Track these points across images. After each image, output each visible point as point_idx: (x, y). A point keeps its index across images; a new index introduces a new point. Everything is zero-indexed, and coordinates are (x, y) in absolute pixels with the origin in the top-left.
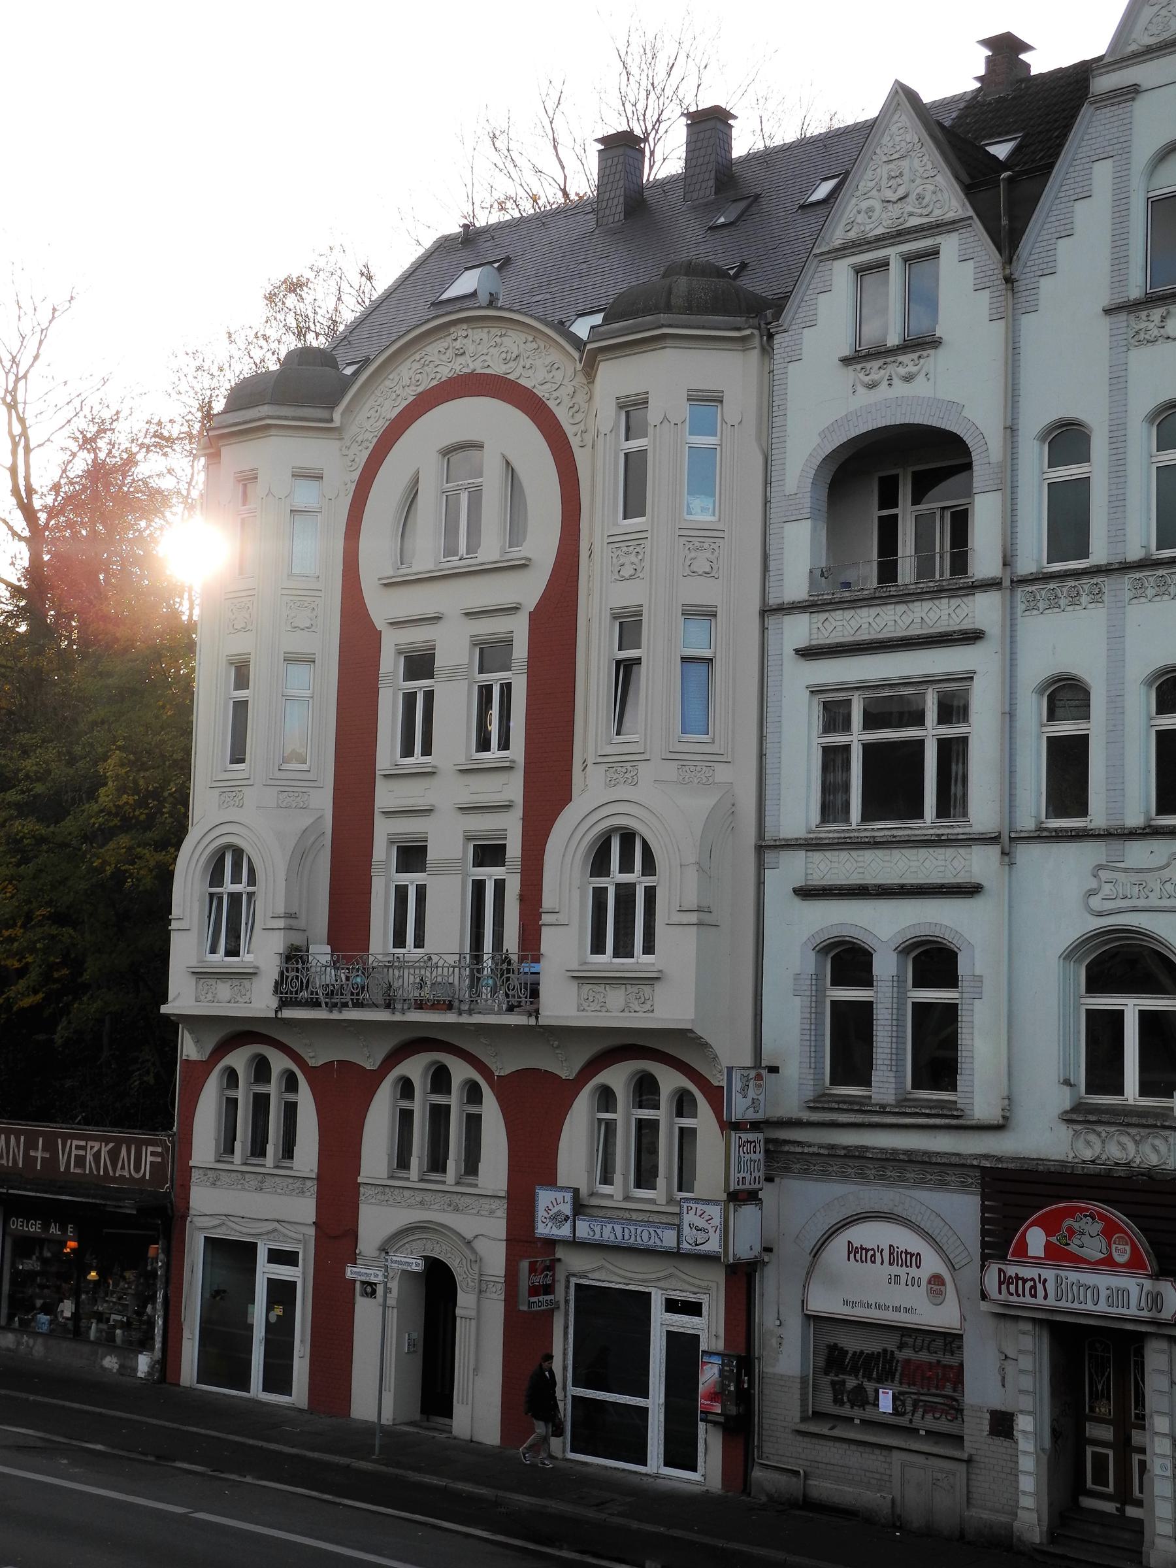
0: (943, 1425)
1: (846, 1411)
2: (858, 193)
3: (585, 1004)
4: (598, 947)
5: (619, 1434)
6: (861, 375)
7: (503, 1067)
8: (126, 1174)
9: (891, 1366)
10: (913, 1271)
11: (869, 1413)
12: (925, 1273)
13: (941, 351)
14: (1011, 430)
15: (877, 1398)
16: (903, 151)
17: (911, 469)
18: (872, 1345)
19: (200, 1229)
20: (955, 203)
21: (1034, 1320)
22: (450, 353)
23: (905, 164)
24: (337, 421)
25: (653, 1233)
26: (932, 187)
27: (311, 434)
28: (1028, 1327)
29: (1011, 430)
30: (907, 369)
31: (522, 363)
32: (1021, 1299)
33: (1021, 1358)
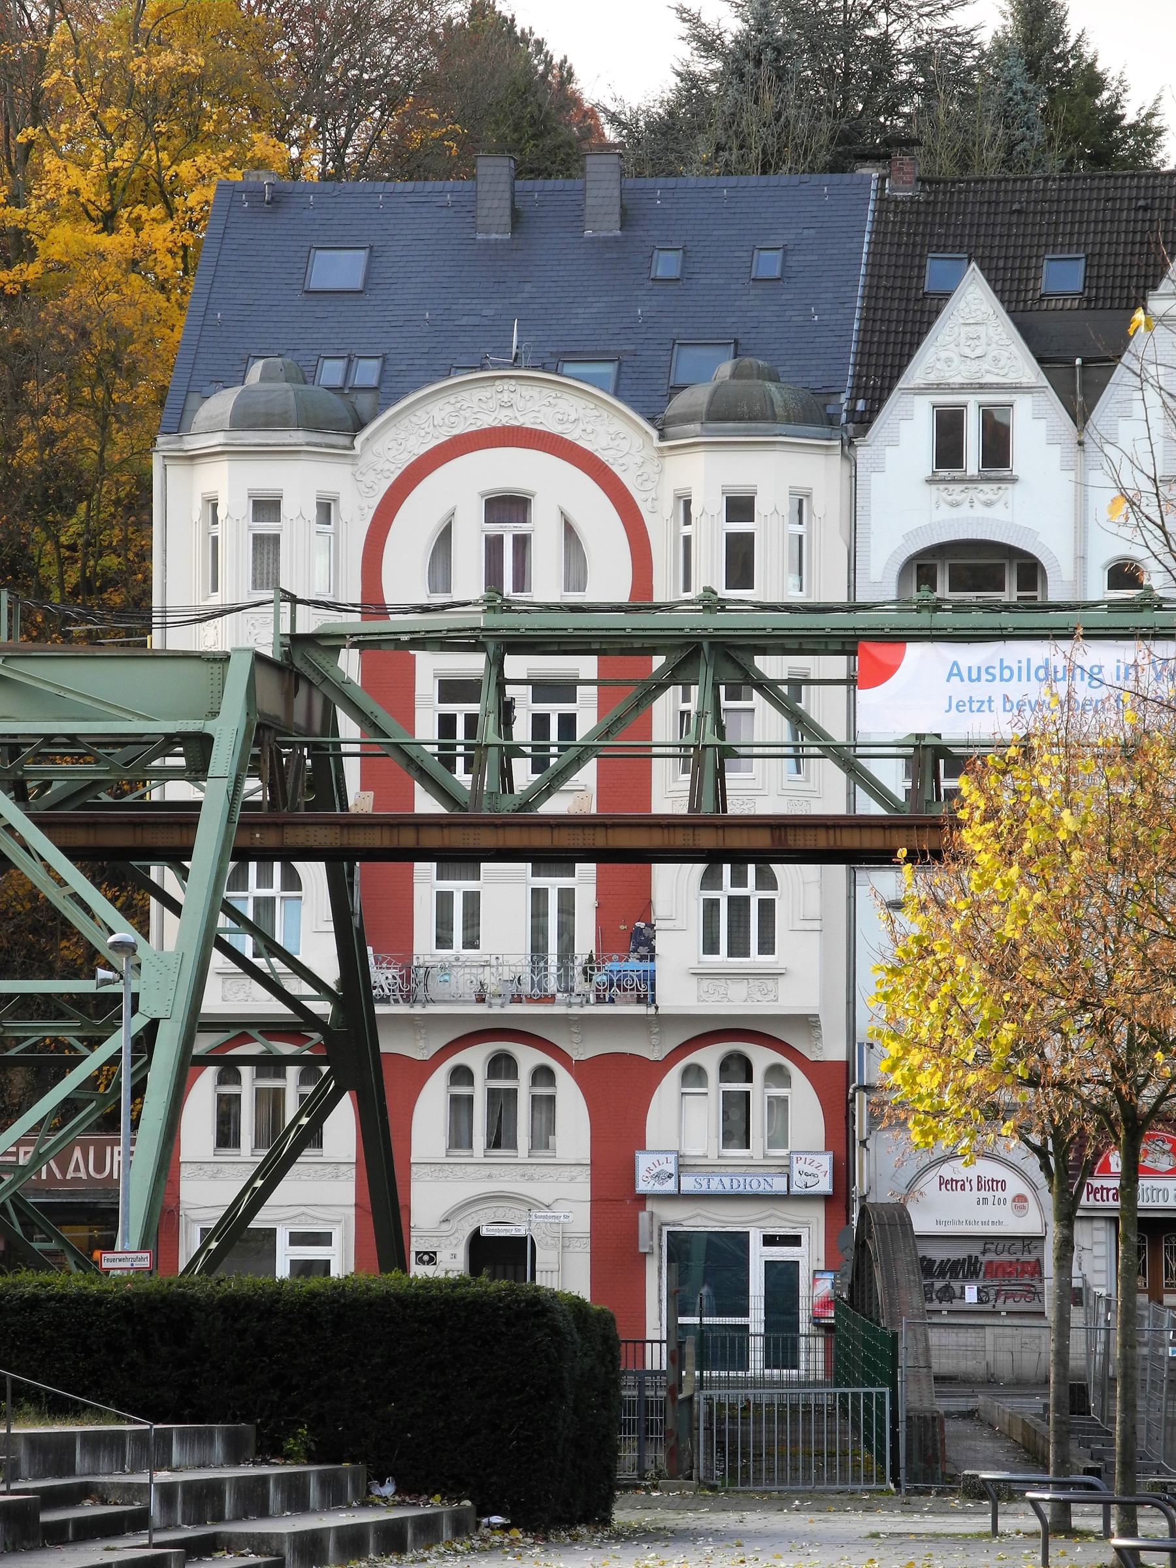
0: (1023, 1306)
1: (935, 1305)
2: (938, 344)
3: (704, 996)
4: (711, 946)
5: (726, 1349)
6: (944, 494)
7: (583, 1050)
8: (83, 1175)
9: (975, 1268)
10: (999, 1194)
11: (956, 1305)
12: (1009, 1194)
13: (1017, 486)
14: (1081, 559)
15: (963, 1293)
16: (979, 319)
17: (948, 562)
18: (958, 1253)
19: (194, 1221)
20: (1028, 371)
21: (1106, 1218)
22: (491, 404)
23: (981, 330)
24: (357, 451)
25: (762, 1182)
26: (1007, 354)
27: (328, 459)
28: (1102, 1224)
29: (1081, 559)
30: (988, 497)
31: (581, 426)
32: (1106, 1203)
33: (1095, 1248)
